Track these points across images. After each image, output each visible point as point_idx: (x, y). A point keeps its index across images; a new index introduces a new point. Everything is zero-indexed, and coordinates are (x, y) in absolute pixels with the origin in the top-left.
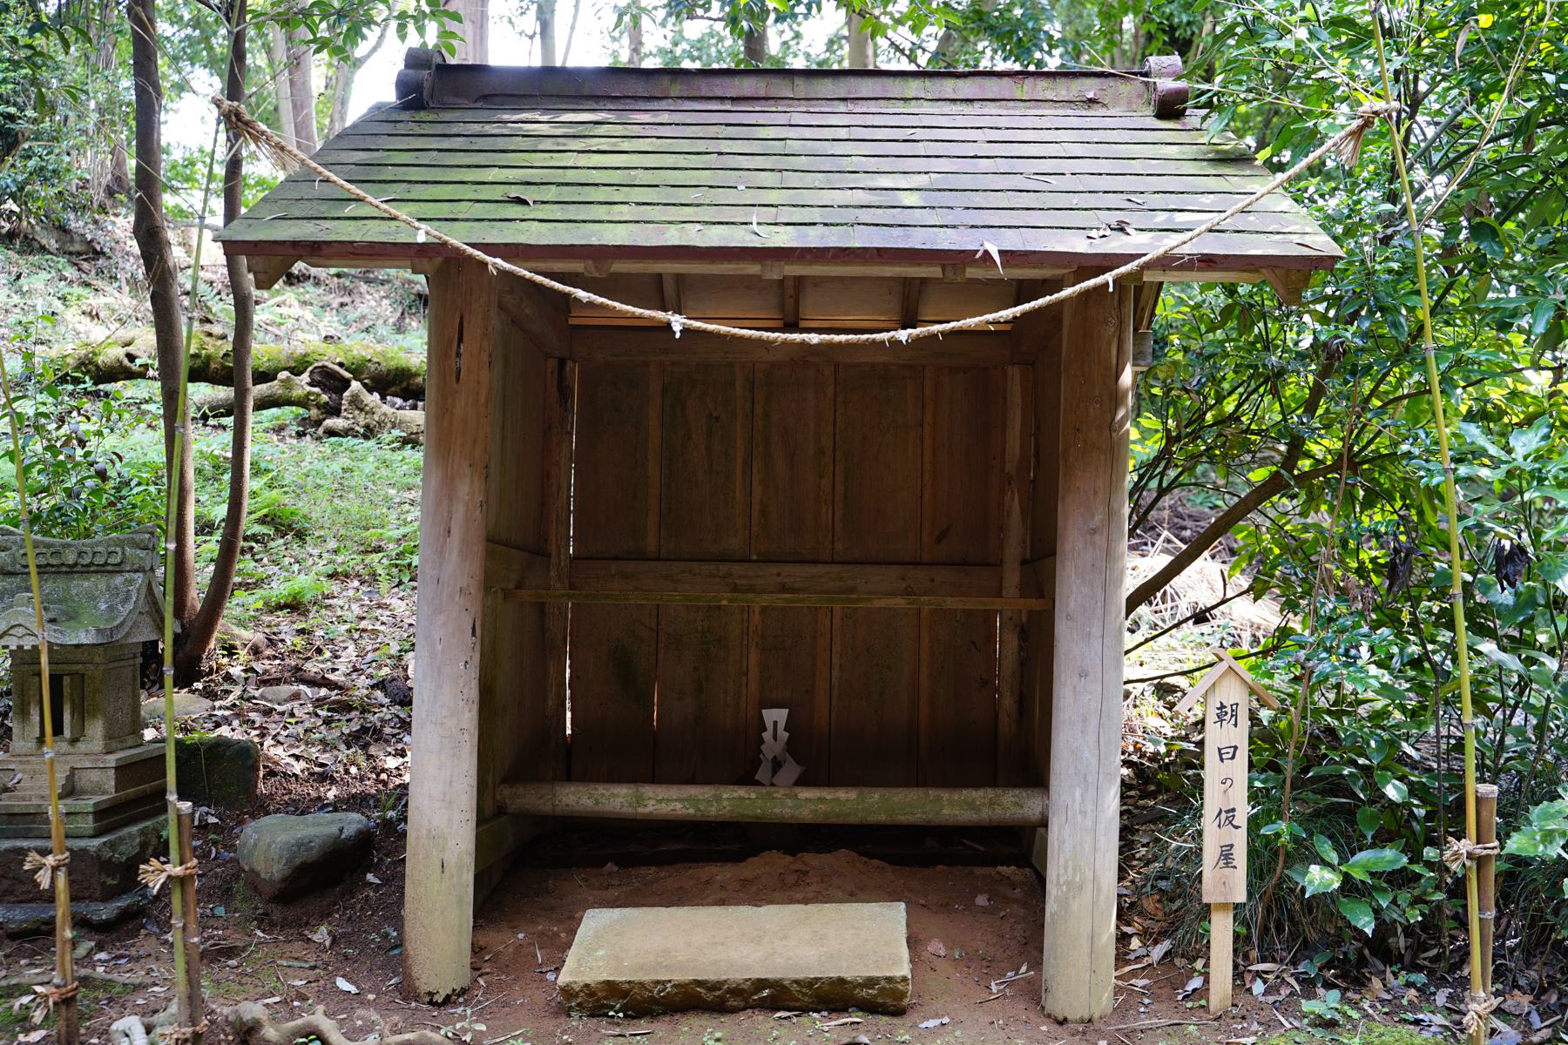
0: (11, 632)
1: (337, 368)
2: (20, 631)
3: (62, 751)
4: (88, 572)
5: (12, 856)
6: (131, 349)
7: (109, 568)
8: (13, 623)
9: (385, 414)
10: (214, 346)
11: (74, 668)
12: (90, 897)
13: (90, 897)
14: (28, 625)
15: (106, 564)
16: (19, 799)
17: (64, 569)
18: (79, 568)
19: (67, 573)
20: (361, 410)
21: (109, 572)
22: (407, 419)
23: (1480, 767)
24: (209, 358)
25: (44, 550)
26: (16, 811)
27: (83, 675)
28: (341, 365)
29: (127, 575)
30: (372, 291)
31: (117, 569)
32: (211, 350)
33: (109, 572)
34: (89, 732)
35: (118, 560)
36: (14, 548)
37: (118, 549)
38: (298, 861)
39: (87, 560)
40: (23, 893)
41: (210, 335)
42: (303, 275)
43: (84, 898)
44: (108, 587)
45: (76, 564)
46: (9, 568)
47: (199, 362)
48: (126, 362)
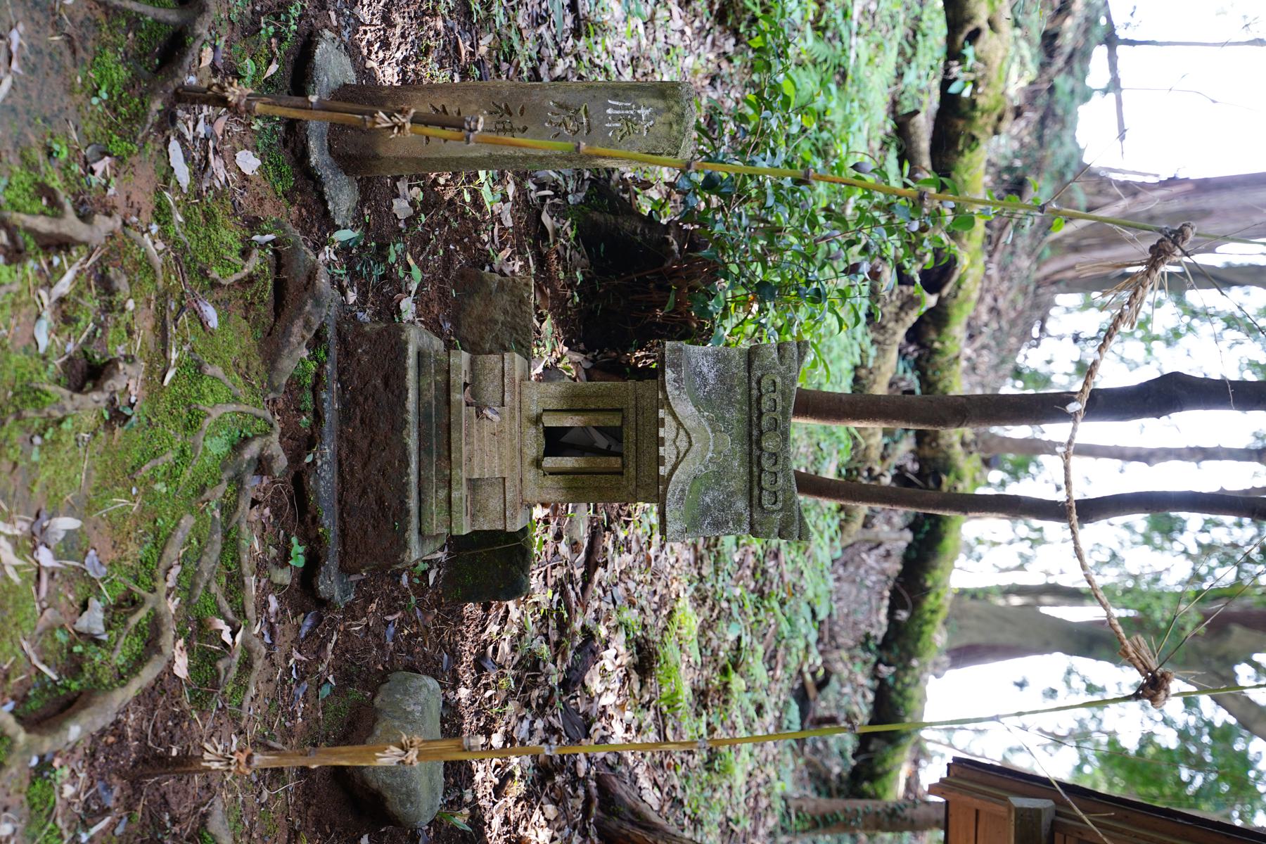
0: (682, 432)
1: (955, 278)
2: (683, 445)
3: (525, 450)
4: (750, 462)
5: (398, 453)
6: (987, 33)
7: (756, 492)
8: (693, 436)
9: (895, 333)
10: (986, 124)
11: (632, 465)
12: (346, 553)
13: (346, 553)
14: (690, 456)
15: (761, 489)
16: (468, 428)
17: (755, 433)
18: (756, 452)
19: (750, 435)
20: (901, 308)
21: (751, 490)
22: (888, 355)
23: (343, 127)
24: (971, 120)
25: (779, 408)
26: (454, 435)
27: (621, 474)
28: (959, 286)
29: (746, 514)
30: (1031, 128)
31: (755, 501)
32: (980, 122)
33: (751, 490)
34: (549, 481)
35: (766, 505)
36: (782, 368)
37: (780, 505)
38: (388, 794)
39: (766, 464)
40: (352, 467)
41: (1000, 119)
42: (1054, 50)
43: (344, 545)
44: (732, 494)
45: (761, 449)
46: (756, 363)
47: (966, 108)
48: (970, 28)
